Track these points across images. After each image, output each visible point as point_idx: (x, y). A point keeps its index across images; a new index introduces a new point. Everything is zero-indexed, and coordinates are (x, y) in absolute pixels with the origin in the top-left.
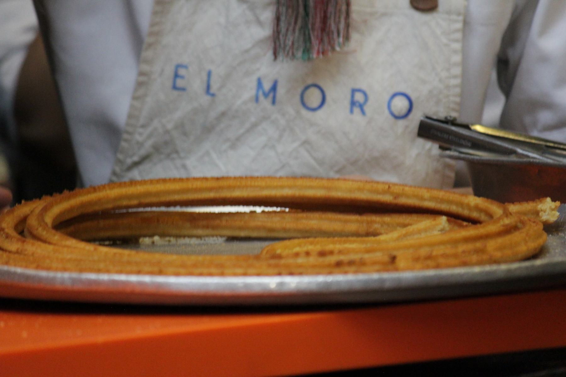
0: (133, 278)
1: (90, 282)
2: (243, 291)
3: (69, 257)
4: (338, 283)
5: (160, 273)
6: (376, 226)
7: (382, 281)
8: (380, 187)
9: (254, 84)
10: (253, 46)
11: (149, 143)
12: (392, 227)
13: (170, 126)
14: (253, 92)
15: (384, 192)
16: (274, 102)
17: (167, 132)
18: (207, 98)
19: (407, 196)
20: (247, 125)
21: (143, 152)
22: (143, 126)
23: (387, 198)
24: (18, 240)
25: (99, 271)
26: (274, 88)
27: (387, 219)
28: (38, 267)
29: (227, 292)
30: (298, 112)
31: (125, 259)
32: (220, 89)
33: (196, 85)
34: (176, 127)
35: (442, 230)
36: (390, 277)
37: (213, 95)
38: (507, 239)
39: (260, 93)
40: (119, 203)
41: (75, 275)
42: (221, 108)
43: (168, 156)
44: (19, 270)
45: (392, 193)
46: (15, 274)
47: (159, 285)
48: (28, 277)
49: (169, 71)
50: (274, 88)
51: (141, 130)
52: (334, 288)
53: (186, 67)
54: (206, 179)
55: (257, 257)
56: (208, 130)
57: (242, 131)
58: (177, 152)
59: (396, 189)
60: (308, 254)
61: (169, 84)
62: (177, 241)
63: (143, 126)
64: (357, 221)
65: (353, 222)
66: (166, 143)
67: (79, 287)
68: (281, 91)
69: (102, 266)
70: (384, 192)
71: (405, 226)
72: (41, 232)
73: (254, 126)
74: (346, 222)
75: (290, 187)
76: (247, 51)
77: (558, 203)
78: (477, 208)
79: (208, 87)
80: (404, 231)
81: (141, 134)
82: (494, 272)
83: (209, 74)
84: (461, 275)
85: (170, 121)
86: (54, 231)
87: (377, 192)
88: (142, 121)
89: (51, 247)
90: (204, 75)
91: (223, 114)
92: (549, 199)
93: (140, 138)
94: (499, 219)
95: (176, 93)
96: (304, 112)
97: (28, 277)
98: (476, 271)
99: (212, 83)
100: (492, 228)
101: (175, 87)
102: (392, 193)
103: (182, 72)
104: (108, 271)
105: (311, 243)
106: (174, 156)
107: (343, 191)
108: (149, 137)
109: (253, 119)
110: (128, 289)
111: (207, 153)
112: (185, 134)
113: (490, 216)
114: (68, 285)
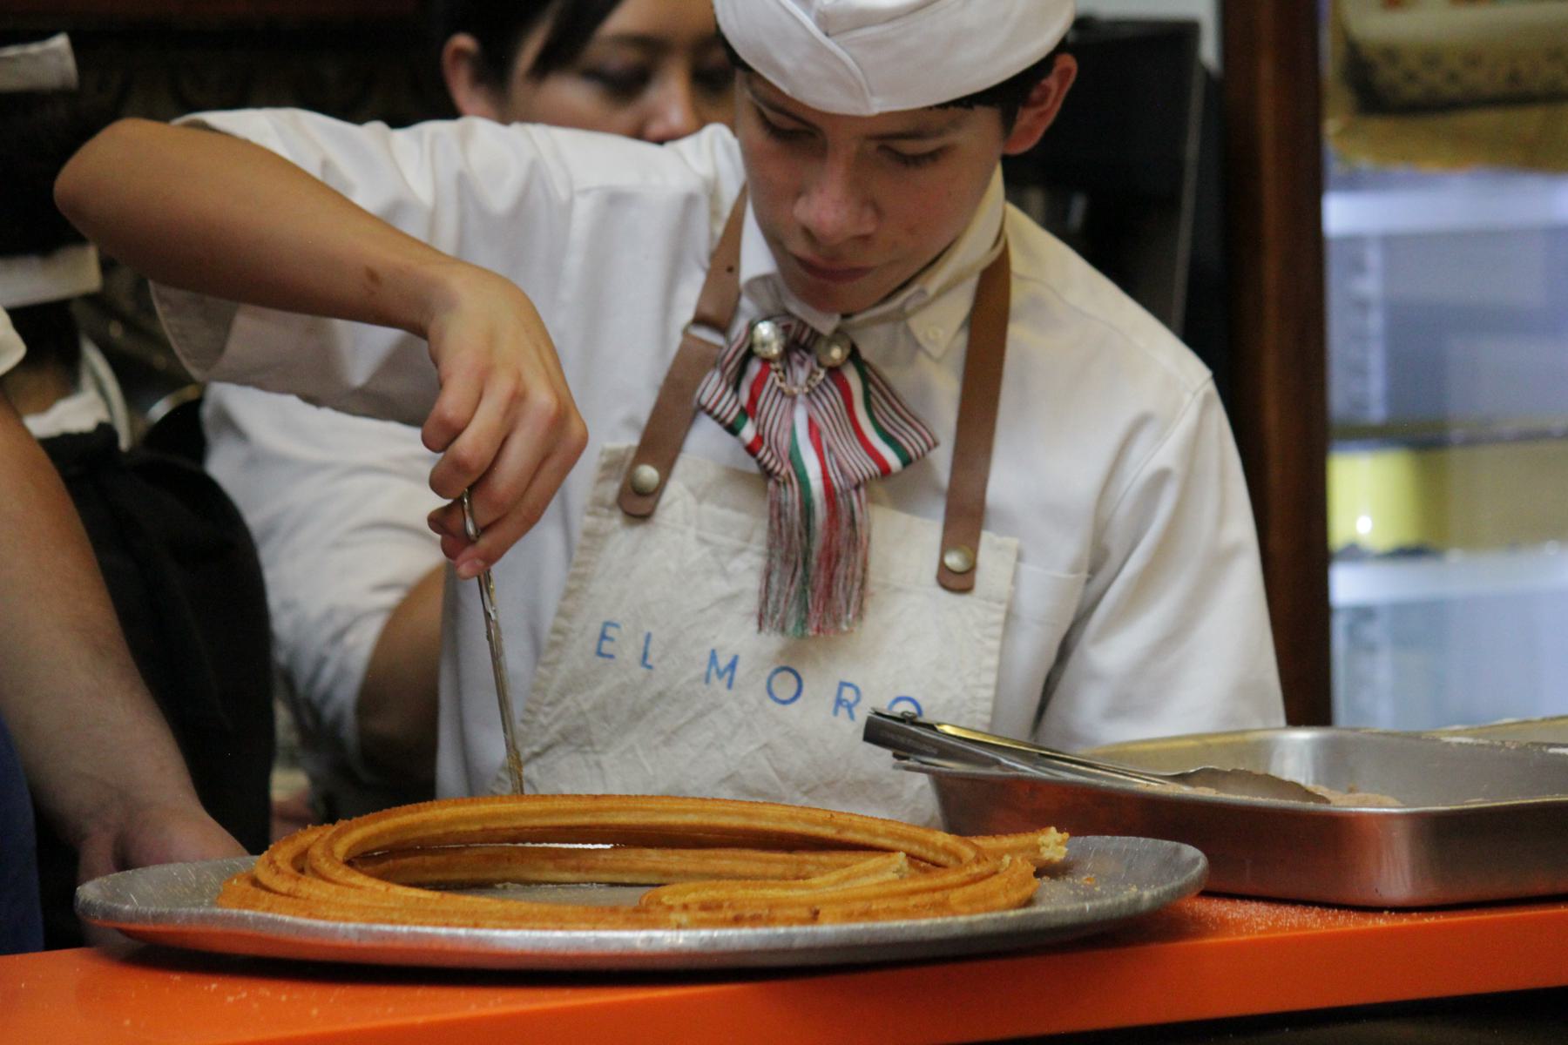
0: (443, 931)
1: (383, 936)
2: (594, 950)
3: (356, 901)
4: (730, 938)
5: (476, 926)
6: (810, 868)
7: (791, 937)
8: (820, 815)
9: (706, 657)
10: (712, 605)
11: (557, 727)
12: (824, 869)
13: (586, 706)
14: (704, 669)
15: (825, 823)
16: (730, 686)
17: (582, 714)
18: (644, 670)
19: (856, 830)
20: (690, 714)
21: (546, 739)
22: (550, 704)
23: (829, 832)
24: (292, 876)
25: (392, 922)
26: (732, 666)
27: (824, 858)
28: (310, 916)
29: (572, 951)
30: (761, 703)
31: (432, 906)
32: (659, 661)
33: (629, 652)
34: (594, 708)
35: (898, 871)
36: (799, 933)
37: (650, 667)
38: (970, 889)
39: (713, 670)
40: (452, 828)
41: (362, 926)
42: (659, 685)
43: (579, 749)
44: (288, 919)
45: (834, 825)
46: (282, 923)
47: (479, 940)
48: (299, 929)
49: (594, 629)
50: (732, 666)
51: (547, 709)
52: (722, 947)
53: (617, 626)
54: (579, 797)
55: (614, 910)
56: (637, 715)
57: (682, 721)
58: (591, 744)
59: (842, 820)
60: (685, 907)
61: (592, 647)
62: (1355, 553)
63: (550, 704)
64: (785, 861)
65: (779, 861)
66: (578, 729)
67: (366, 943)
68: (741, 670)
69: (395, 916)
70: (825, 823)
71: (845, 866)
72: (325, 866)
73: (701, 715)
74: (769, 862)
75: (695, 812)
76: (702, 611)
77: (1066, 835)
78: (945, 850)
79: (645, 656)
80: (845, 872)
81: (546, 715)
82: (949, 926)
83: (648, 637)
84: (902, 930)
85: (585, 701)
86: (345, 868)
87: (815, 823)
88: (550, 697)
89: (333, 888)
90: (641, 639)
91: (661, 695)
92: (1053, 829)
93: (543, 720)
94: (969, 864)
95: (600, 660)
96: (769, 702)
97: (299, 928)
98: (927, 924)
99: (650, 650)
100: (952, 878)
101: (600, 653)
102: (834, 825)
103: (611, 632)
104: (404, 923)
105: (713, 888)
106: (588, 748)
107: (769, 820)
108: (557, 719)
109: (699, 706)
110: (436, 946)
111: (632, 749)
112: (606, 719)
113: (959, 859)
114: (354, 940)
